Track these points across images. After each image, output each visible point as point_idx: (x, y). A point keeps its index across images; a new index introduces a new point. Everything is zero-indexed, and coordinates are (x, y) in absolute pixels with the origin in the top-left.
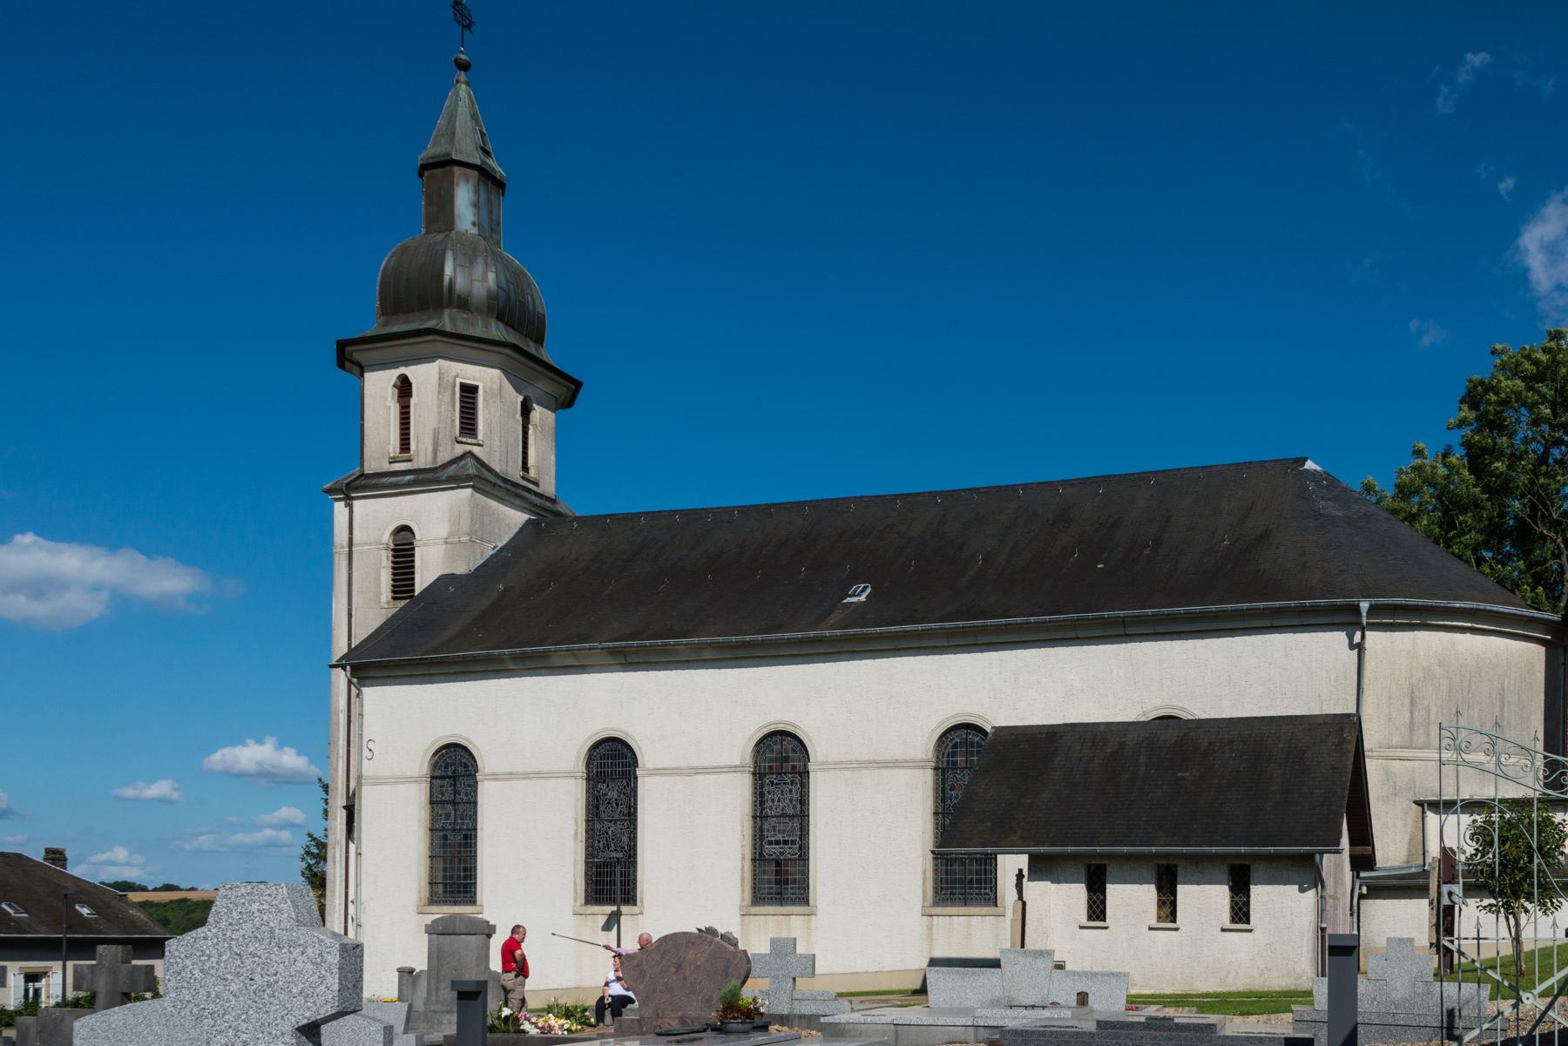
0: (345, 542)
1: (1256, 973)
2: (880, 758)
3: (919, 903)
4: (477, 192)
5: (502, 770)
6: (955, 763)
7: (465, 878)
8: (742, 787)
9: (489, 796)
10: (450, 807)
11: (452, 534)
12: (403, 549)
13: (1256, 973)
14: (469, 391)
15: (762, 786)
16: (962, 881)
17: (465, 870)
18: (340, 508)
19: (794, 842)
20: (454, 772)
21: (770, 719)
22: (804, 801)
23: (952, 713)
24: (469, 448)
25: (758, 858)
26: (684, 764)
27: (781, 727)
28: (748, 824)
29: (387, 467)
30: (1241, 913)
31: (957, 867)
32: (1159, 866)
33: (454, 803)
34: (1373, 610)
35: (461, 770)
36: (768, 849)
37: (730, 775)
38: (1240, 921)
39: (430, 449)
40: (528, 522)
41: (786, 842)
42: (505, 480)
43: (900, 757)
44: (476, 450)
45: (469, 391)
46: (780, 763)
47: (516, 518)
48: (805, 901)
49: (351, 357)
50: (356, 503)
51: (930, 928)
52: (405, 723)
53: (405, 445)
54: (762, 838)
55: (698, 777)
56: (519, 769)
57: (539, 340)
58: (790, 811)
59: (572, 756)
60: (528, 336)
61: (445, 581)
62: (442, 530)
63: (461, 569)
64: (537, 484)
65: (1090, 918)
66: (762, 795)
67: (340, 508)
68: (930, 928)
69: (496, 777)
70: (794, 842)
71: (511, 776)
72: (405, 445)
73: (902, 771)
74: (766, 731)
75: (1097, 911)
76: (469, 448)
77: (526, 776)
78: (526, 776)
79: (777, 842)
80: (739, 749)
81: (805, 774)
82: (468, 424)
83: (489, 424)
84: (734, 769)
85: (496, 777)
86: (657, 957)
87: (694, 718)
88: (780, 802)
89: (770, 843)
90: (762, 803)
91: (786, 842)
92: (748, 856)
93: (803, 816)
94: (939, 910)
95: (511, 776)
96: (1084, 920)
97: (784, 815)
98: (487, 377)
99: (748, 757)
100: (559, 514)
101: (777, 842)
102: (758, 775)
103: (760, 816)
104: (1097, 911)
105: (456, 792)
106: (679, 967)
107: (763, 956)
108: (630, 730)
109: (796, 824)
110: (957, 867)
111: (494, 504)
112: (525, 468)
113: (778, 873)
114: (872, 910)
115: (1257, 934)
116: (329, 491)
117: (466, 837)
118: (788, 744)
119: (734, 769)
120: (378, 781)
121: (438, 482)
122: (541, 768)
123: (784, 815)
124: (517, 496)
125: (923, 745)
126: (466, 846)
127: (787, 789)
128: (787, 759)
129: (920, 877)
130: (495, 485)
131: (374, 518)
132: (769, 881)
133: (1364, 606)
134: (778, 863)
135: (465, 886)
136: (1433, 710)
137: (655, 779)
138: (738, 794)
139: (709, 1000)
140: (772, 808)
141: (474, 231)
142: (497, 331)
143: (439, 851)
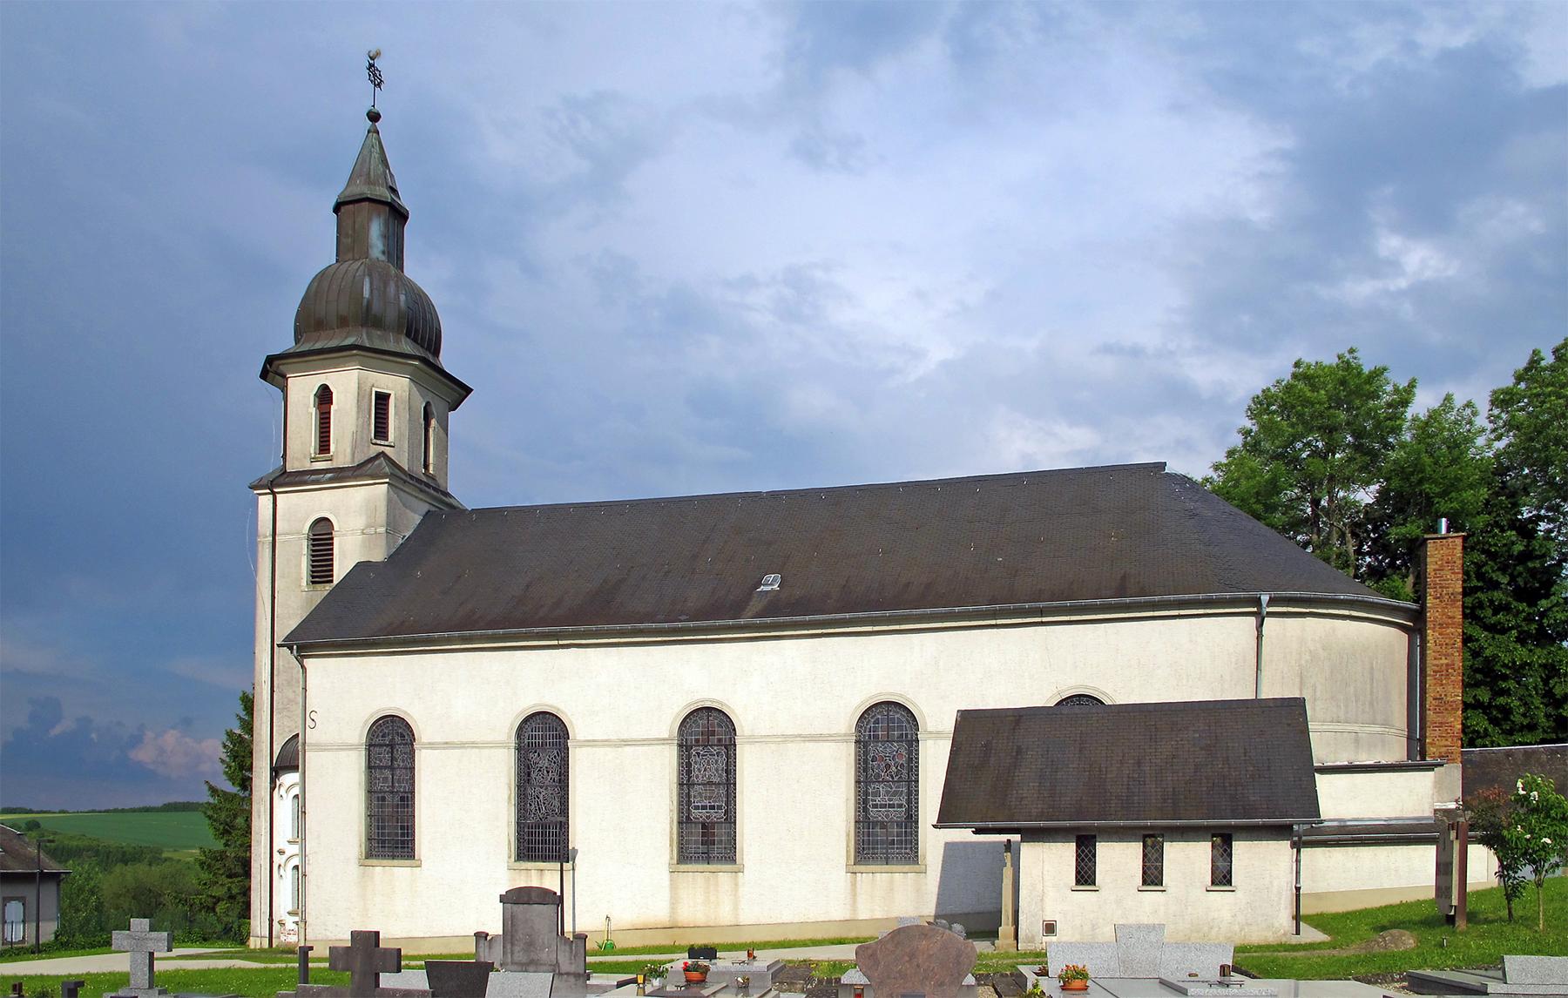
0: (269, 531)
1: (1237, 928)
3: (844, 861)
4: (387, 225)
5: (438, 740)
6: (876, 737)
7: (403, 835)
8: (668, 758)
9: (427, 765)
10: (388, 773)
11: (369, 526)
12: (321, 538)
13: (1237, 928)
14: (382, 399)
15: (689, 757)
16: (882, 842)
17: (402, 828)
18: (265, 502)
19: (720, 807)
20: (391, 743)
24: (382, 449)
27: (708, 704)
29: (308, 466)
30: (1222, 877)
33: (392, 768)
34: (1272, 602)
35: (398, 739)
37: (660, 747)
39: (349, 450)
41: (712, 807)
42: (412, 477)
43: (825, 732)
44: (388, 450)
45: (382, 399)
46: (707, 739)
49: (274, 370)
51: (854, 884)
52: (345, 694)
53: (324, 446)
54: (689, 803)
55: (627, 749)
57: (436, 353)
60: (428, 349)
61: (361, 567)
62: (359, 522)
63: (378, 555)
66: (689, 765)
67: (265, 502)
68: (854, 884)
69: (432, 746)
70: (720, 807)
71: (447, 745)
72: (324, 446)
75: (1085, 876)
76: (382, 449)
77: (462, 745)
78: (462, 745)
79: (704, 807)
80: (667, 724)
82: (381, 431)
83: (397, 428)
85: (432, 746)
89: (697, 808)
91: (712, 807)
93: (730, 784)
95: (447, 745)
97: (710, 783)
98: (398, 385)
101: (704, 807)
102: (685, 748)
103: (686, 782)
104: (1085, 876)
105: (393, 759)
108: (561, 706)
109: (722, 791)
112: (426, 466)
113: (704, 835)
114: (800, 872)
115: (1239, 894)
116: (253, 487)
117: (402, 799)
120: (322, 748)
122: (474, 739)
125: (846, 722)
126: (403, 806)
129: (844, 838)
131: (297, 510)
132: (696, 842)
133: (1265, 598)
134: (704, 826)
135: (403, 842)
136: (1319, 688)
140: (698, 775)
141: (383, 258)
142: (407, 346)
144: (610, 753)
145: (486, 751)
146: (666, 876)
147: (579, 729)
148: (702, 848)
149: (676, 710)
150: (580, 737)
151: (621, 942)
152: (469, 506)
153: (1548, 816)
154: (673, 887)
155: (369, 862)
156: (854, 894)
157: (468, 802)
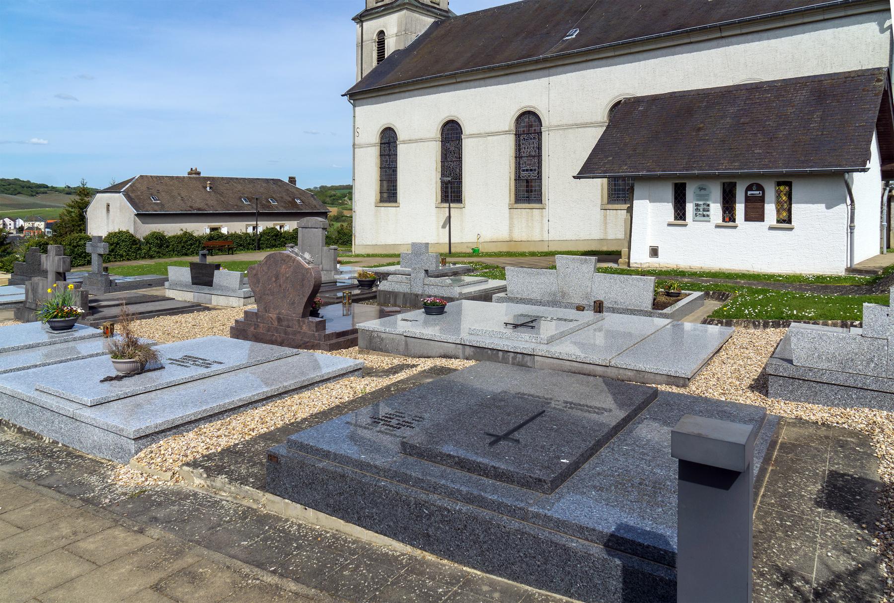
2: (578, 122)
3: (599, 202)
8: (510, 140)
16: (624, 190)
19: (535, 170)
21: (523, 105)
22: (540, 148)
23: (617, 94)
25: (518, 179)
26: (482, 131)
28: (513, 161)
31: (620, 182)
32: (724, 184)
33: (389, 155)
36: (523, 174)
38: (784, 221)
40: (435, 23)
41: (531, 170)
47: (429, 21)
48: (540, 201)
50: (364, 24)
51: (605, 216)
55: (489, 138)
56: (413, 138)
58: (533, 154)
59: (435, 131)
61: (397, 52)
63: (402, 47)
64: (438, 4)
65: (676, 218)
66: (519, 145)
68: (605, 216)
69: (404, 142)
70: (535, 170)
73: (590, 129)
74: (521, 112)
79: (527, 170)
80: (508, 123)
81: (540, 134)
84: (506, 133)
86: (265, 268)
87: (487, 108)
88: (451, 146)
90: (519, 150)
91: (531, 170)
92: (513, 177)
94: (610, 206)
96: (671, 219)
97: (530, 156)
99: (513, 127)
100: (448, 17)
101: (527, 170)
102: (518, 135)
103: (518, 157)
105: (390, 150)
106: (277, 278)
107: (408, 254)
110: (620, 182)
111: (417, 15)
113: (527, 186)
118: (532, 118)
119: (506, 133)
121: (393, 8)
122: (422, 137)
123: (530, 156)
124: (428, 11)
127: (531, 141)
128: (531, 126)
130: (417, 7)
134: (527, 181)
137: (470, 140)
138: (508, 144)
139: (293, 303)
143: (384, 178)
144: (481, 140)
145: (426, 143)
146: (507, 210)
147: (467, 129)
148: (526, 194)
149: (513, 113)
150: (467, 133)
151: (483, 249)
152: (458, 14)
153: (185, 574)
154: (511, 218)
155: (381, 204)
156: (605, 223)
157: (489, 166)
